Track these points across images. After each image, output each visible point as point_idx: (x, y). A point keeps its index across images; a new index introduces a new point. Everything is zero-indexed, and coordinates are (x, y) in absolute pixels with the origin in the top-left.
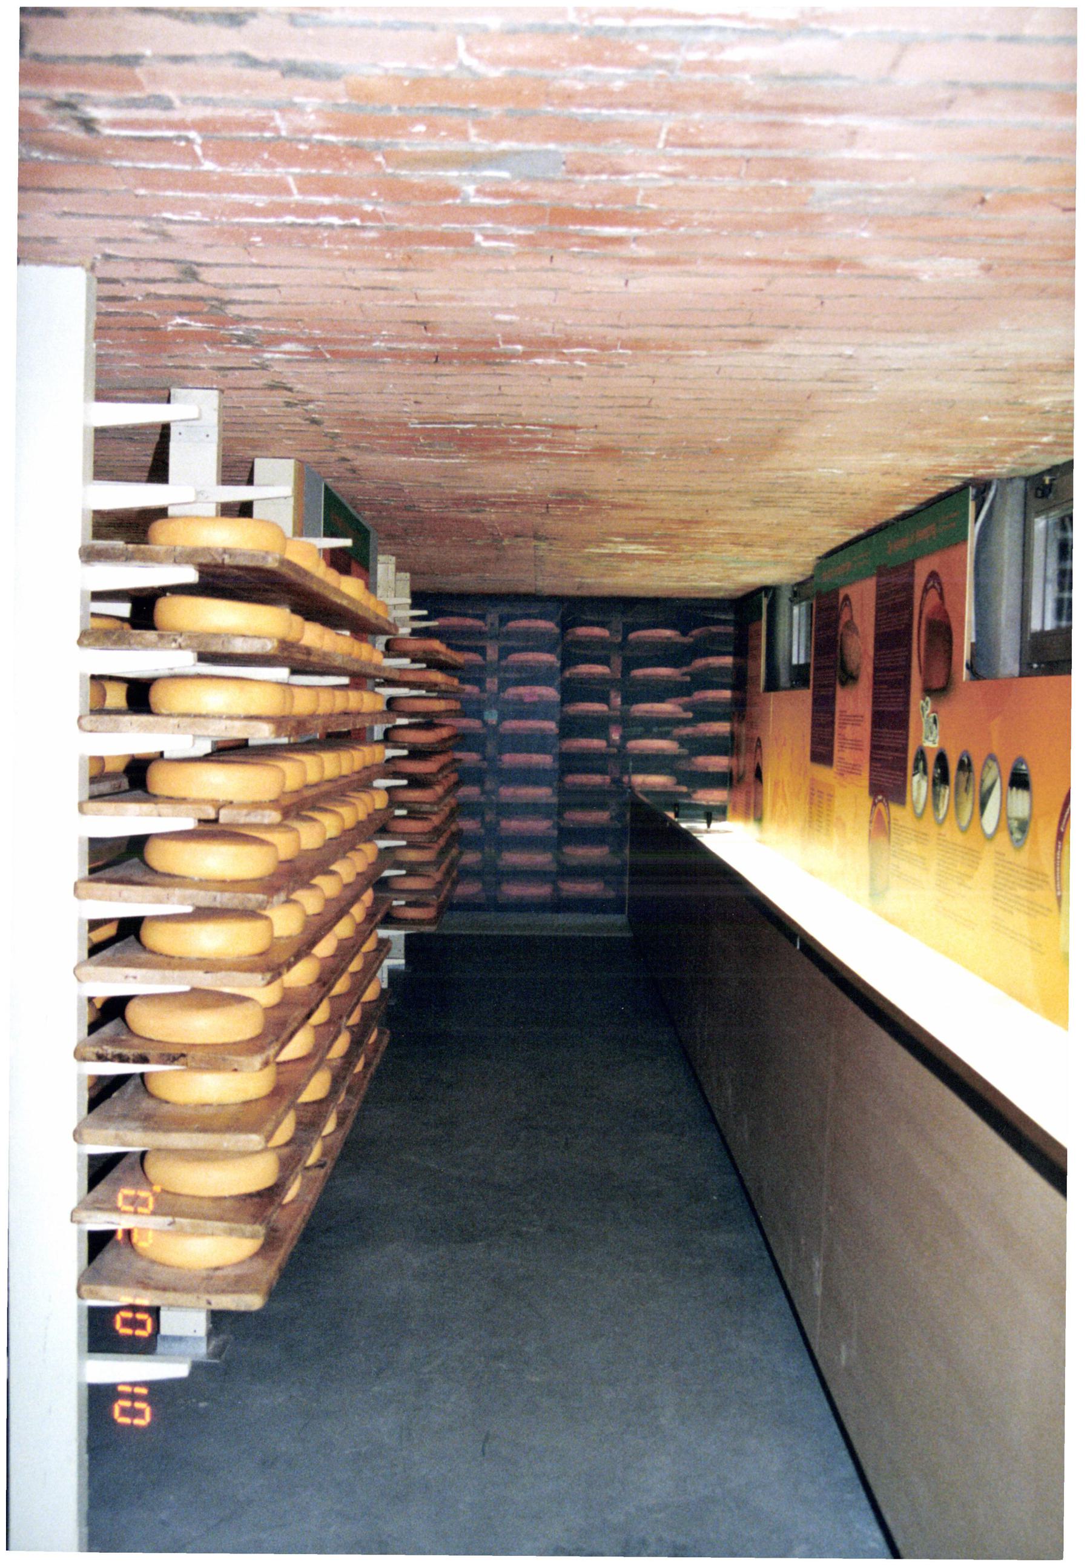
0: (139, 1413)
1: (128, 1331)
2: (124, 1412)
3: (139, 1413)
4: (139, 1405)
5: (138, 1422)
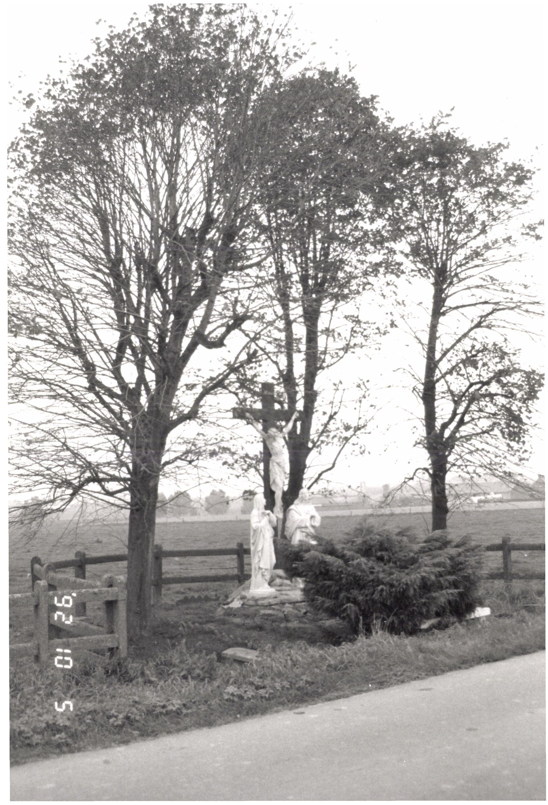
0: (68, 663)
1: (60, 666)
2: (60, 662)
3: (68, 663)
4: (67, 658)
5: (66, 667)
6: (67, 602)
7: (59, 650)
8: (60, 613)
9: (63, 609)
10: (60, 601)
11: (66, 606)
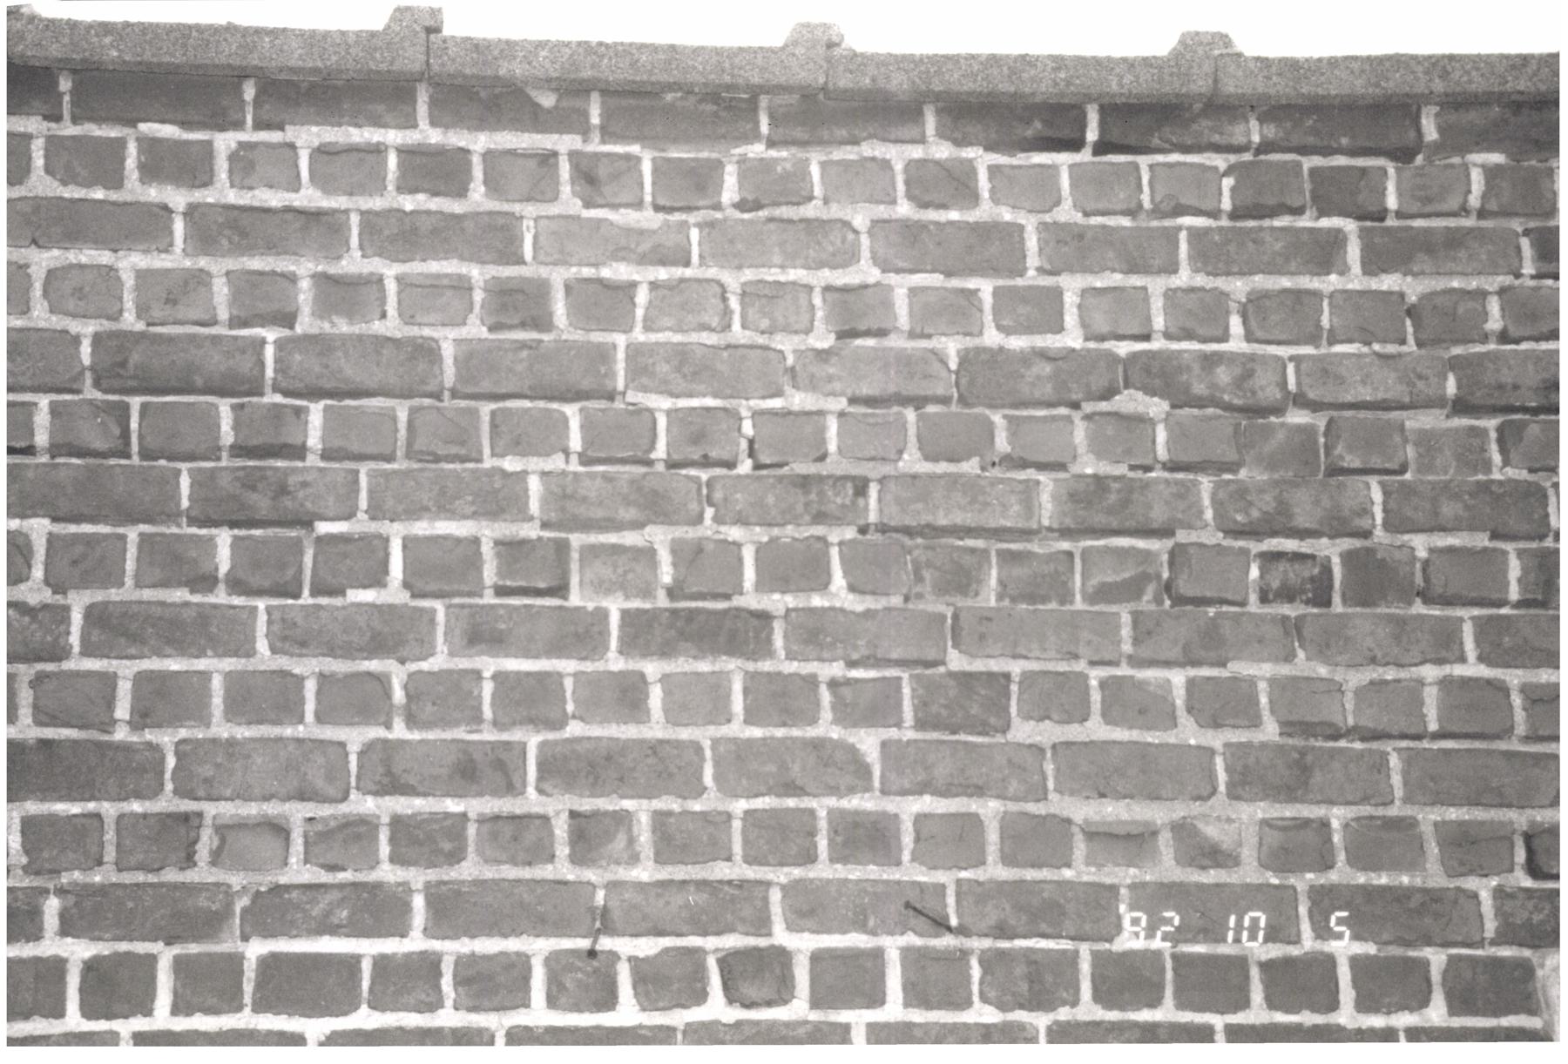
0: (1255, 921)
3: (1255, 921)
4: (1247, 923)
5: (1262, 924)
11: (1144, 923)
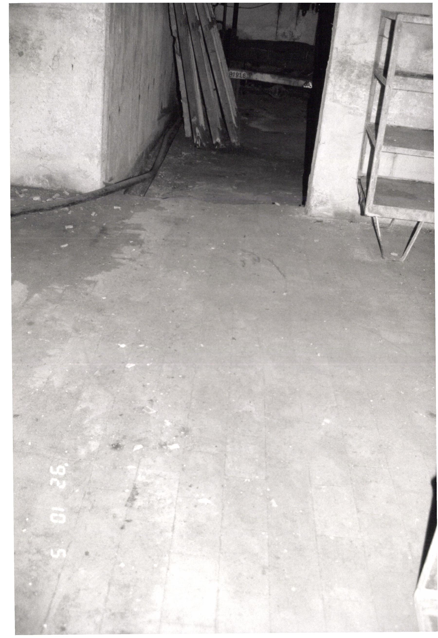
0: (61, 519)
2: (55, 518)
3: (61, 519)
6: (61, 471)
7: (54, 509)
8: (56, 480)
9: (57, 477)
10: (55, 470)
